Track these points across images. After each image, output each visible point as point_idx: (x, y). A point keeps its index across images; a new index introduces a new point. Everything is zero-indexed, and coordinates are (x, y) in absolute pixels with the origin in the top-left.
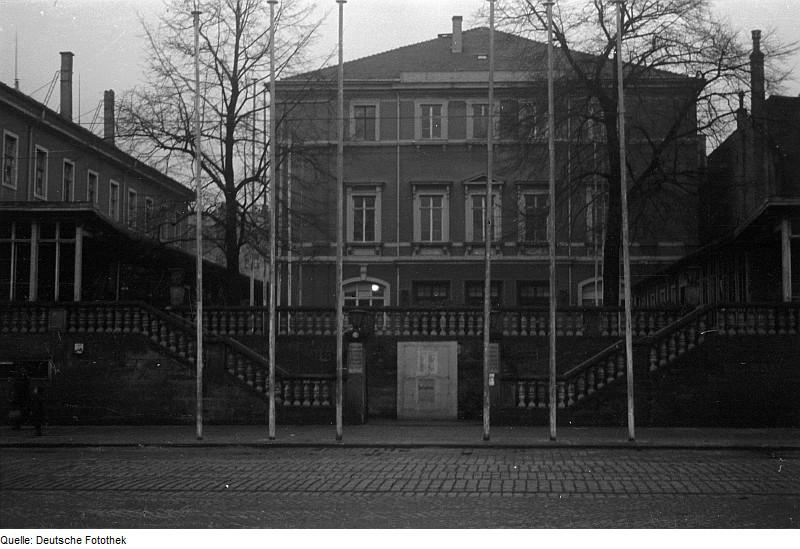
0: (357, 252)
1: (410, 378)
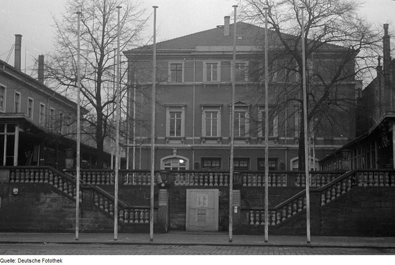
0: (171, 142)
1: (193, 209)
